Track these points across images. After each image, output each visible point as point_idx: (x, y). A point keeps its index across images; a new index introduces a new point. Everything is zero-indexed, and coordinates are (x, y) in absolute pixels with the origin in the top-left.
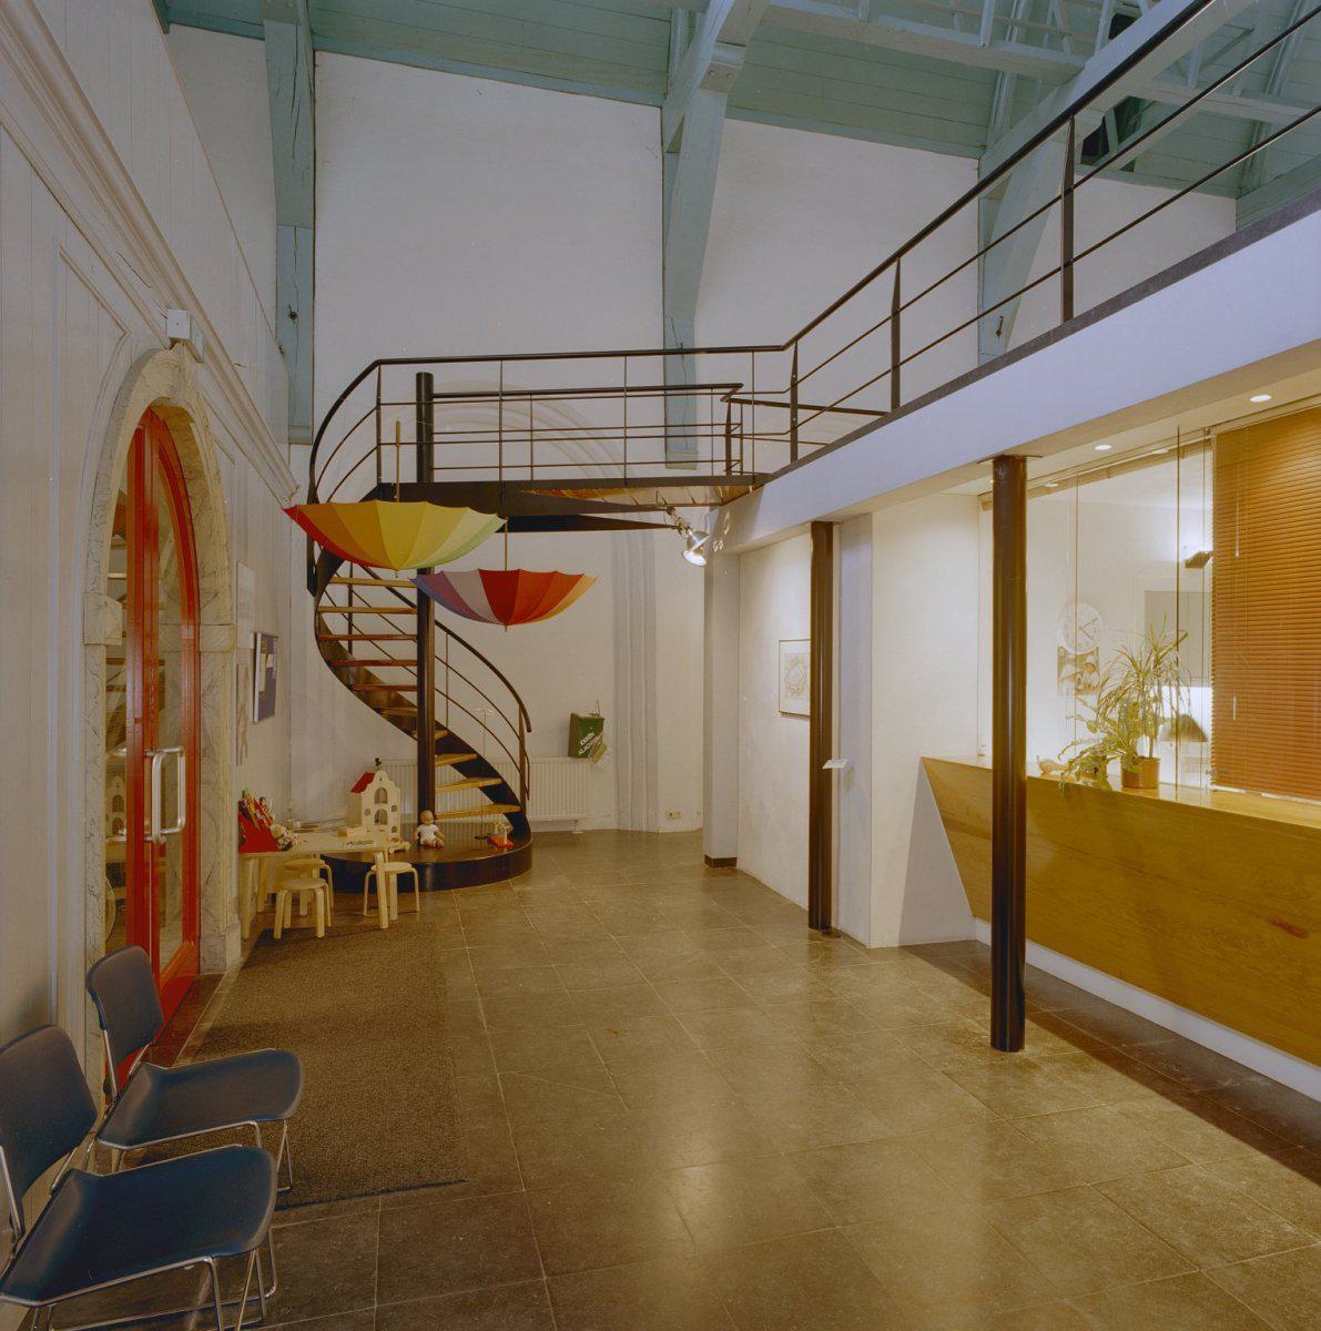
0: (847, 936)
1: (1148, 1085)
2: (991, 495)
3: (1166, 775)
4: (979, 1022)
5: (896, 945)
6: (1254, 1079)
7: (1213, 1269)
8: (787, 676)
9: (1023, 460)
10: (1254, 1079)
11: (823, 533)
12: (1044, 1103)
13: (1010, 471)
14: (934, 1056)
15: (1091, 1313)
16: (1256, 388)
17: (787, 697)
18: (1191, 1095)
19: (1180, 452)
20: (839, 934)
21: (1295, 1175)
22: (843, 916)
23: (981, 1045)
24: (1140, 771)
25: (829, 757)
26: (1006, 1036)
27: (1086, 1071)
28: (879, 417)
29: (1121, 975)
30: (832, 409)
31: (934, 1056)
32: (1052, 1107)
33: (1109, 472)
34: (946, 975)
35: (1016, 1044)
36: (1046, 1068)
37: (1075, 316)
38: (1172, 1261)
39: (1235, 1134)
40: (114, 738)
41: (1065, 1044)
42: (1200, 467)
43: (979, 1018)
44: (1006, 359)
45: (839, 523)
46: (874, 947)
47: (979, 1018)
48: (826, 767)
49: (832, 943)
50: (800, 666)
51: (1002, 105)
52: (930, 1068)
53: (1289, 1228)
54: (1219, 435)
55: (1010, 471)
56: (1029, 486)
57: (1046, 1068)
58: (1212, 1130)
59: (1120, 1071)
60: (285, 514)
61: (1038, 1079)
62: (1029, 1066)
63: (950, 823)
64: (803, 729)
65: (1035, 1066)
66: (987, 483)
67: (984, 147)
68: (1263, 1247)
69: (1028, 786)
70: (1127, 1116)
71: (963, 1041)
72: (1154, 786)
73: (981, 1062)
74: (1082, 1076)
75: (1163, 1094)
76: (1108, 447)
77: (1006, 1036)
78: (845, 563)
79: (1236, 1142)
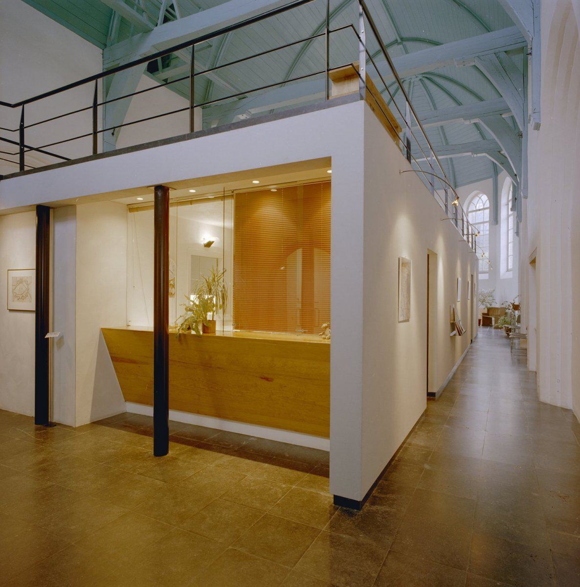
0: (59, 424)
1: (220, 452)
2: (153, 203)
3: (218, 328)
4: (144, 447)
5: (89, 423)
6: (251, 439)
7: (270, 510)
8: (13, 290)
9: (168, 189)
10: (251, 439)
11: (44, 215)
12: (187, 472)
13: (162, 193)
14: (131, 468)
15: (240, 547)
16: (255, 178)
17: (13, 301)
18: (235, 451)
19: (223, 198)
20: (53, 425)
21: (278, 468)
22: (57, 415)
23: (150, 456)
24: (208, 327)
25: (47, 332)
26: (161, 450)
27: (196, 454)
28: (65, 161)
29: (198, 412)
30: (37, 150)
31: (131, 468)
32: (191, 473)
33: (191, 202)
34: (120, 431)
35: (165, 452)
36: (181, 458)
37: (195, 131)
38: (257, 513)
39: (255, 460)
40: (131, 207)
41: (184, 446)
42: (230, 204)
43: (144, 445)
44: (163, 142)
45: (53, 208)
46: (77, 426)
47: (144, 445)
48: (46, 337)
49: (49, 429)
50: (25, 284)
51: (114, 28)
52: (132, 474)
53: (284, 486)
54: (236, 194)
55: (162, 193)
56: (170, 201)
57: (181, 458)
58: (247, 461)
59: (208, 450)
60: (166, 24)
61: (180, 463)
62: (174, 459)
63: (114, 359)
64: (31, 319)
65: (176, 459)
66: (151, 197)
67: (105, 45)
68: (280, 496)
69: (169, 336)
70: (219, 467)
71: (141, 457)
72: (214, 332)
73: (153, 464)
74: (196, 457)
75: (227, 454)
76: (142, 199)
77: (161, 450)
78: (59, 231)
79: (255, 463)
